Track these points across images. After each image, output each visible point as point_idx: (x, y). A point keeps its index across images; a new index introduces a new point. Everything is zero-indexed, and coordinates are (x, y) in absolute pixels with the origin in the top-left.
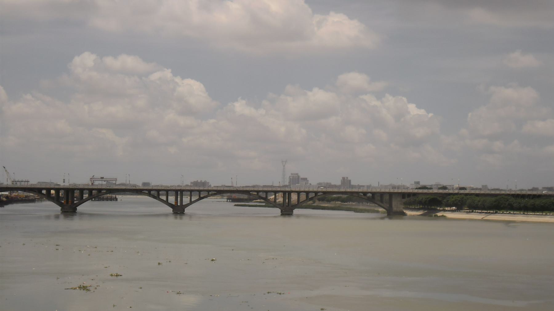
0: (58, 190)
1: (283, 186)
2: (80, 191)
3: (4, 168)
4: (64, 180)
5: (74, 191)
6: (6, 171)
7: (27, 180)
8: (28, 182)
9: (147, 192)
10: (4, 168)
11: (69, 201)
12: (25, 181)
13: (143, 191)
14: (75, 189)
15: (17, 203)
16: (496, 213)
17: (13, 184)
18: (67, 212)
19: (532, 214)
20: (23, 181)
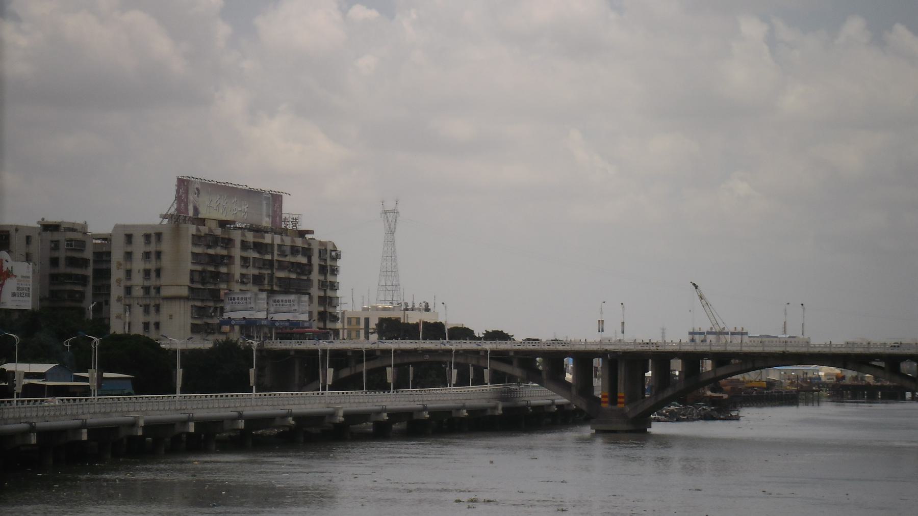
0: (584, 358)
1: (719, 332)
2: (712, 361)
3: (696, 287)
4: (601, 322)
5: (899, 365)
6: (701, 297)
7: (739, 330)
8: (743, 334)
9: (882, 364)
10: (696, 287)
11: (619, 394)
12: (733, 334)
13: (874, 363)
14: (567, 354)
15: (757, 406)
16: (516, 435)
17: (693, 340)
18: (615, 432)
19: (414, 443)
20: (727, 333)
